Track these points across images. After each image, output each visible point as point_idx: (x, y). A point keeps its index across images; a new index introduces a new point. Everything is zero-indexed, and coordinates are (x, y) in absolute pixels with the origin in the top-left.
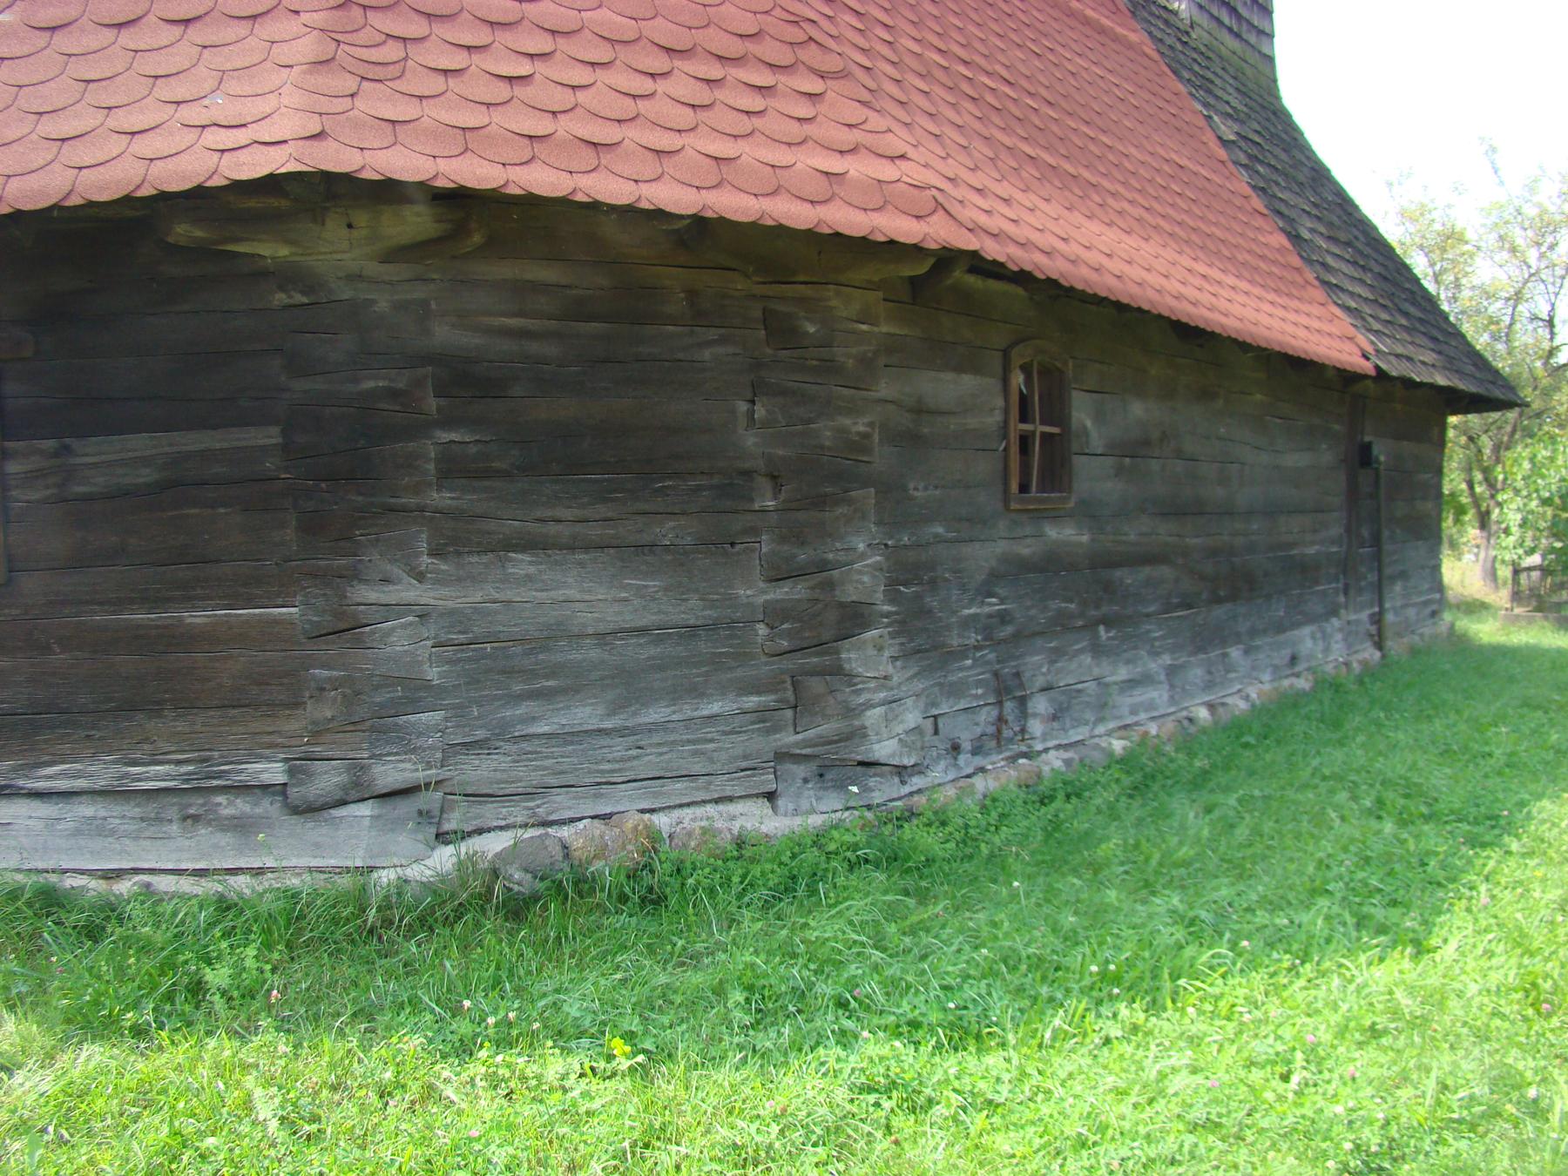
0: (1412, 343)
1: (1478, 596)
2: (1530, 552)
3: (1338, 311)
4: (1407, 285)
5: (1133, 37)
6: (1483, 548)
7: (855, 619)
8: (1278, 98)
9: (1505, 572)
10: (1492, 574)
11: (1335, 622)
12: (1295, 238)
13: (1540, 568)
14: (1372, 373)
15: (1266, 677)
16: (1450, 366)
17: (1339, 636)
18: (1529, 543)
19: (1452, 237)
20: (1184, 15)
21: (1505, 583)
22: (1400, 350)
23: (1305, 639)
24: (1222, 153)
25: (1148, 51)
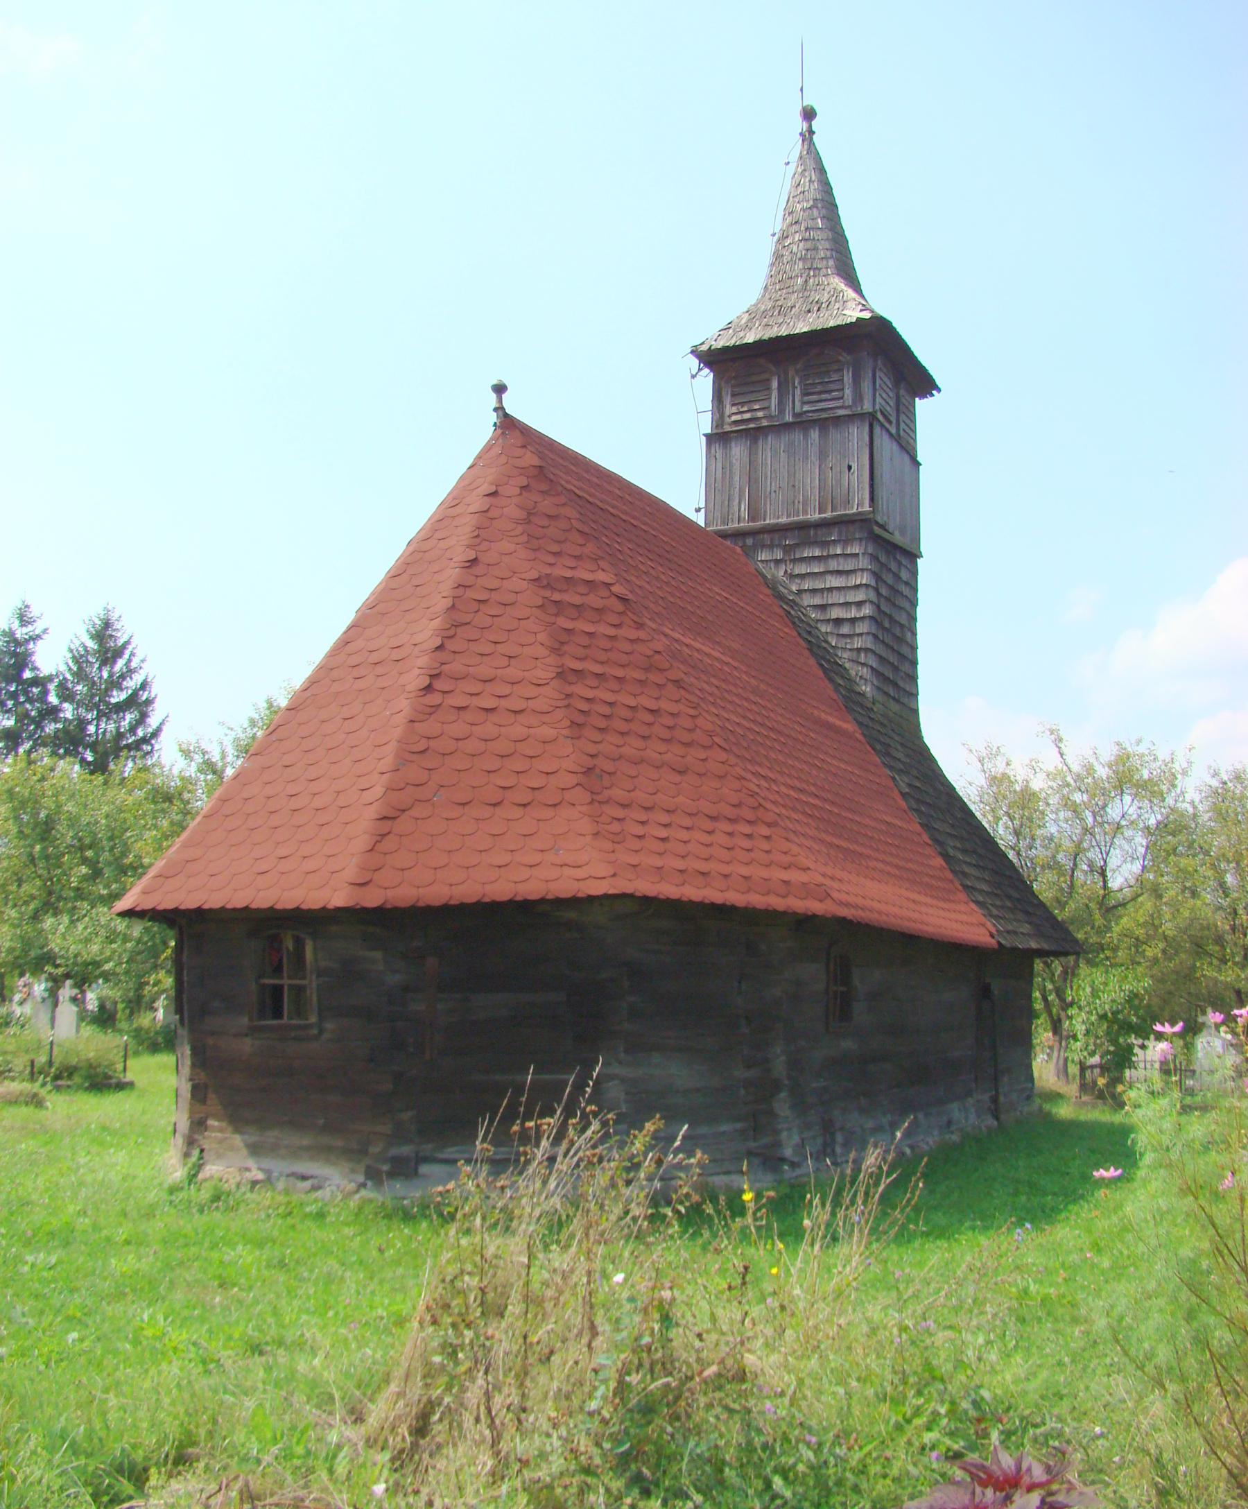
0: (1015, 920)
1: (1054, 1088)
2: (1092, 1054)
3: (973, 906)
4: (1008, 873)
5: (845, 726)
6: (1056, 1049)
7: (776, 1086)
8: (920, 738)
9: (1074, 1070)
10: (1063, 1071)
11: (970, 1101)
12: (946, 856)
13: (1101, 1066)
14: (996, 946)
15: (936, 1132)
16: (1039, 933)
17: (973, 1110)
18: (1091, 1047)
19: (1027, 798)
20: (869, 695)
21: (1074, 1078)
22: (1010, 928)
23: (955, 1110)
24: (902, 803)
25: (858, 735)
